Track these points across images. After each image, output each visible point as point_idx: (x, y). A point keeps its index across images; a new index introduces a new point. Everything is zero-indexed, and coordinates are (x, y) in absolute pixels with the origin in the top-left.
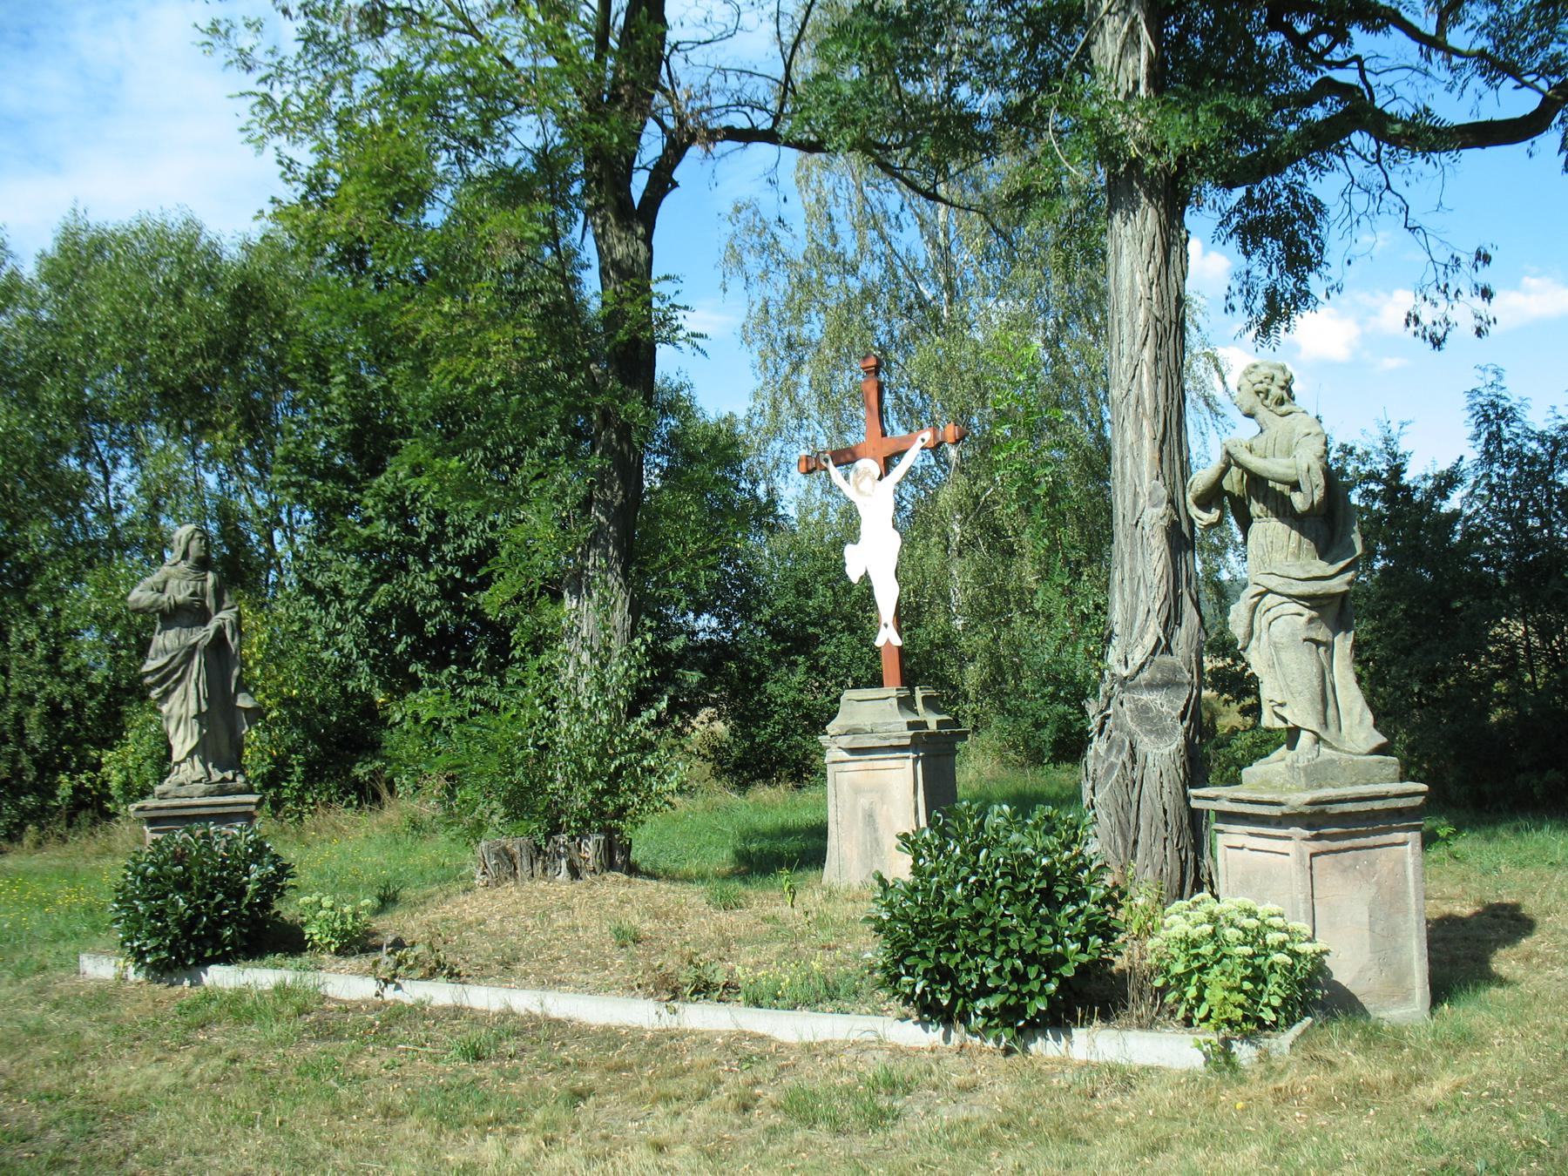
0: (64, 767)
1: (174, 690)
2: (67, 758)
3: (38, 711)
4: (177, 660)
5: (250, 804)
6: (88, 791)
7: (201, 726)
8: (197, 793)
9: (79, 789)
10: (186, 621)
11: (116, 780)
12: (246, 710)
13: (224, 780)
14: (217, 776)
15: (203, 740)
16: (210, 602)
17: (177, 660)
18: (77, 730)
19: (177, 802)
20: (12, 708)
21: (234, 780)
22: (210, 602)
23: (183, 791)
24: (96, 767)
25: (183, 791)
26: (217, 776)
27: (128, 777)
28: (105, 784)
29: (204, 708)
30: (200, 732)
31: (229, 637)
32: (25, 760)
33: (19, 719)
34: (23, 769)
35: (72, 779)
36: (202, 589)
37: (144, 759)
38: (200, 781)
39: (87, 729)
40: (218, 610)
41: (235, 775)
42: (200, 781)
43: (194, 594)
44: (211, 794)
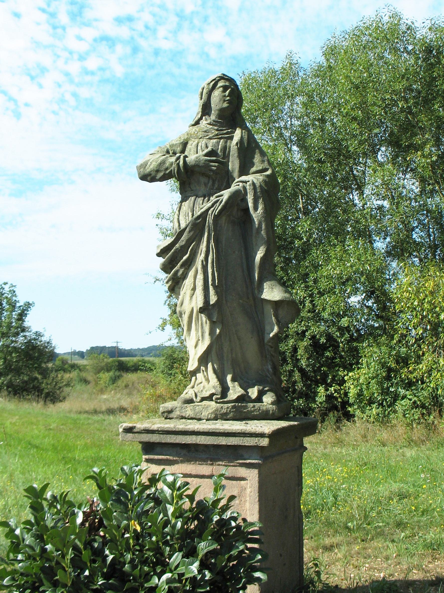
0: (323, 381)
1: (184, 276)
2: (325, 375)
3: (305, 344)
4: (184, 238)
5: (262, 435)
6: (336, 398)
7: (213, 325)
8: (205, 414)
9: (330, 397)
10: (203, 190)
11: (353, 392)
12: (277, 304)
13: (243, 398)
14: (235, 391)
15: (216, 341)
16: (234, 164)
17: (184, 238)
18: (334, 358)
19: (181, 425)
20: (291, 342)
21: (259, 399)
22: (234, 164)
23: (189, 411)
24: (342, 382)
25: (189, 411)
26: (235, 391)
27: (361, 390)
28: (346, 394)
29: (213, 299)
30: (212, 333)
31: (251, 205)
32: (297, 376)
33: (295, 349)
34: (295, 382)
35: (327, 390)
36: (225, 148)
37: (373, 378)
38: (210, 398)
39: (341, 357)
40: (244, 171)
41: (261, 393)
42: (210, 398)
43: (212, 153)
44: (224, 417)
